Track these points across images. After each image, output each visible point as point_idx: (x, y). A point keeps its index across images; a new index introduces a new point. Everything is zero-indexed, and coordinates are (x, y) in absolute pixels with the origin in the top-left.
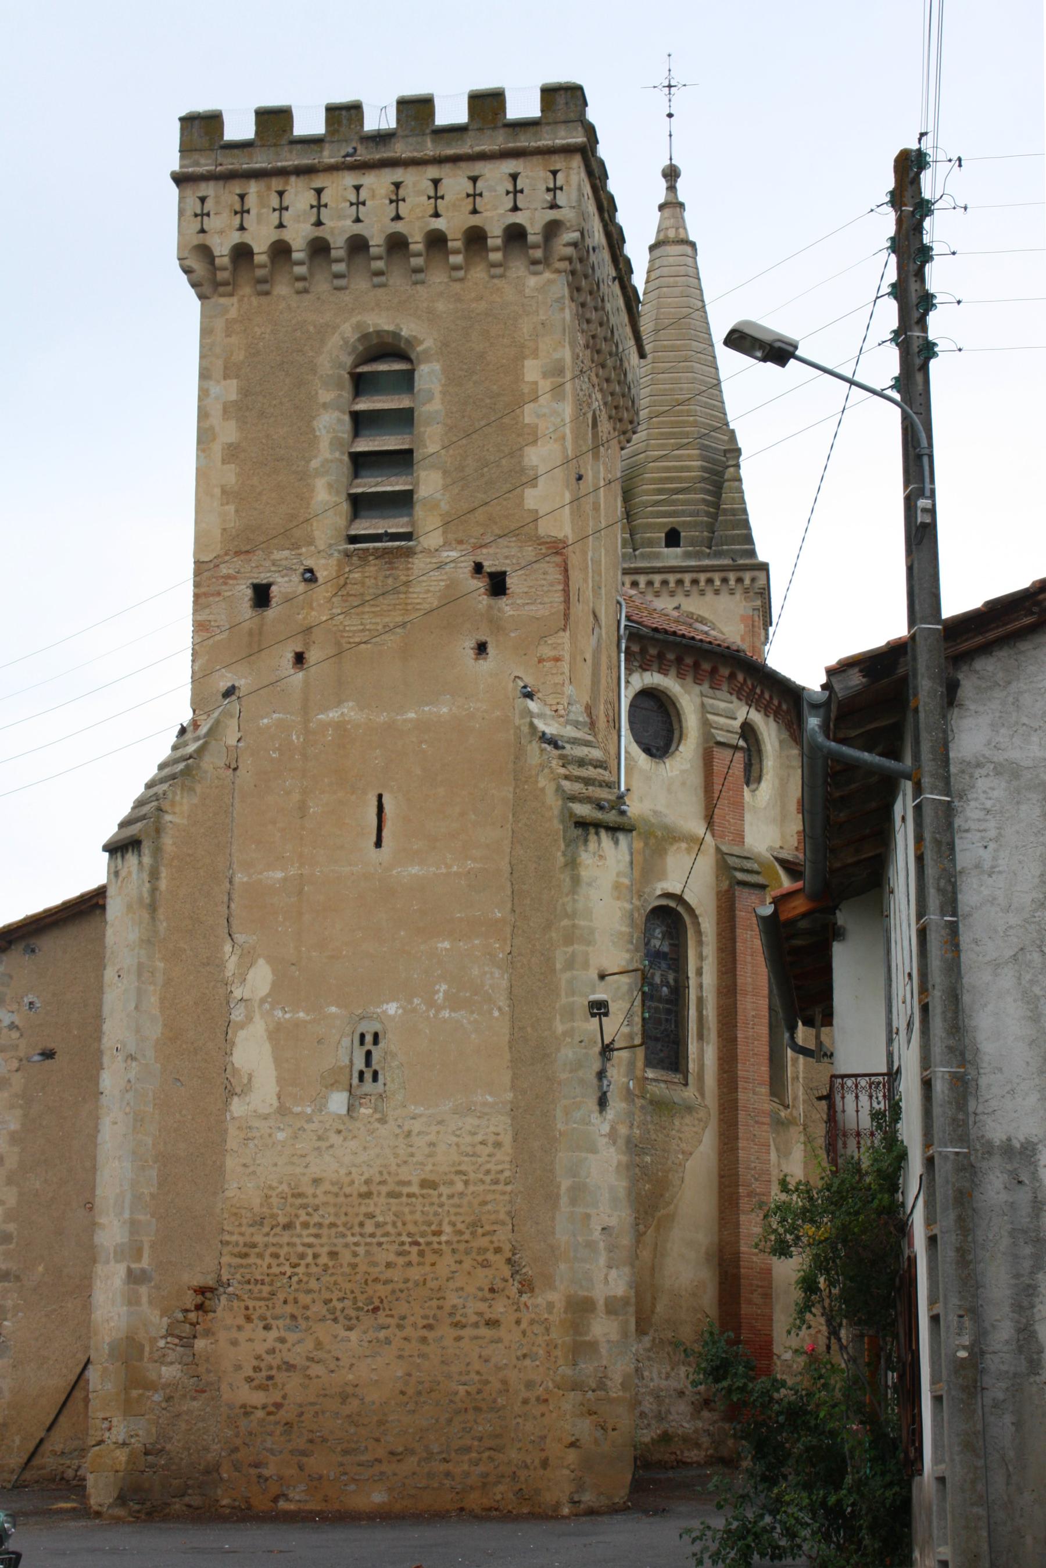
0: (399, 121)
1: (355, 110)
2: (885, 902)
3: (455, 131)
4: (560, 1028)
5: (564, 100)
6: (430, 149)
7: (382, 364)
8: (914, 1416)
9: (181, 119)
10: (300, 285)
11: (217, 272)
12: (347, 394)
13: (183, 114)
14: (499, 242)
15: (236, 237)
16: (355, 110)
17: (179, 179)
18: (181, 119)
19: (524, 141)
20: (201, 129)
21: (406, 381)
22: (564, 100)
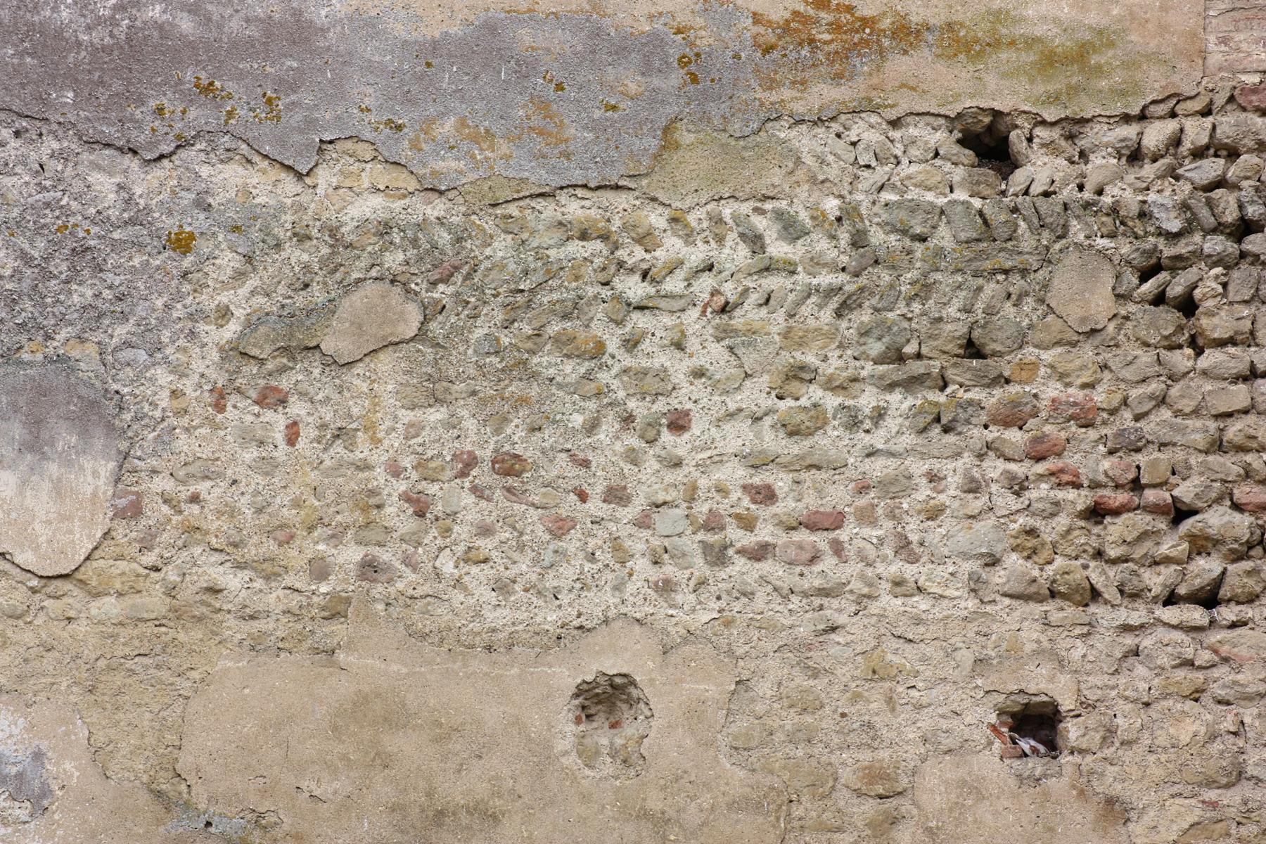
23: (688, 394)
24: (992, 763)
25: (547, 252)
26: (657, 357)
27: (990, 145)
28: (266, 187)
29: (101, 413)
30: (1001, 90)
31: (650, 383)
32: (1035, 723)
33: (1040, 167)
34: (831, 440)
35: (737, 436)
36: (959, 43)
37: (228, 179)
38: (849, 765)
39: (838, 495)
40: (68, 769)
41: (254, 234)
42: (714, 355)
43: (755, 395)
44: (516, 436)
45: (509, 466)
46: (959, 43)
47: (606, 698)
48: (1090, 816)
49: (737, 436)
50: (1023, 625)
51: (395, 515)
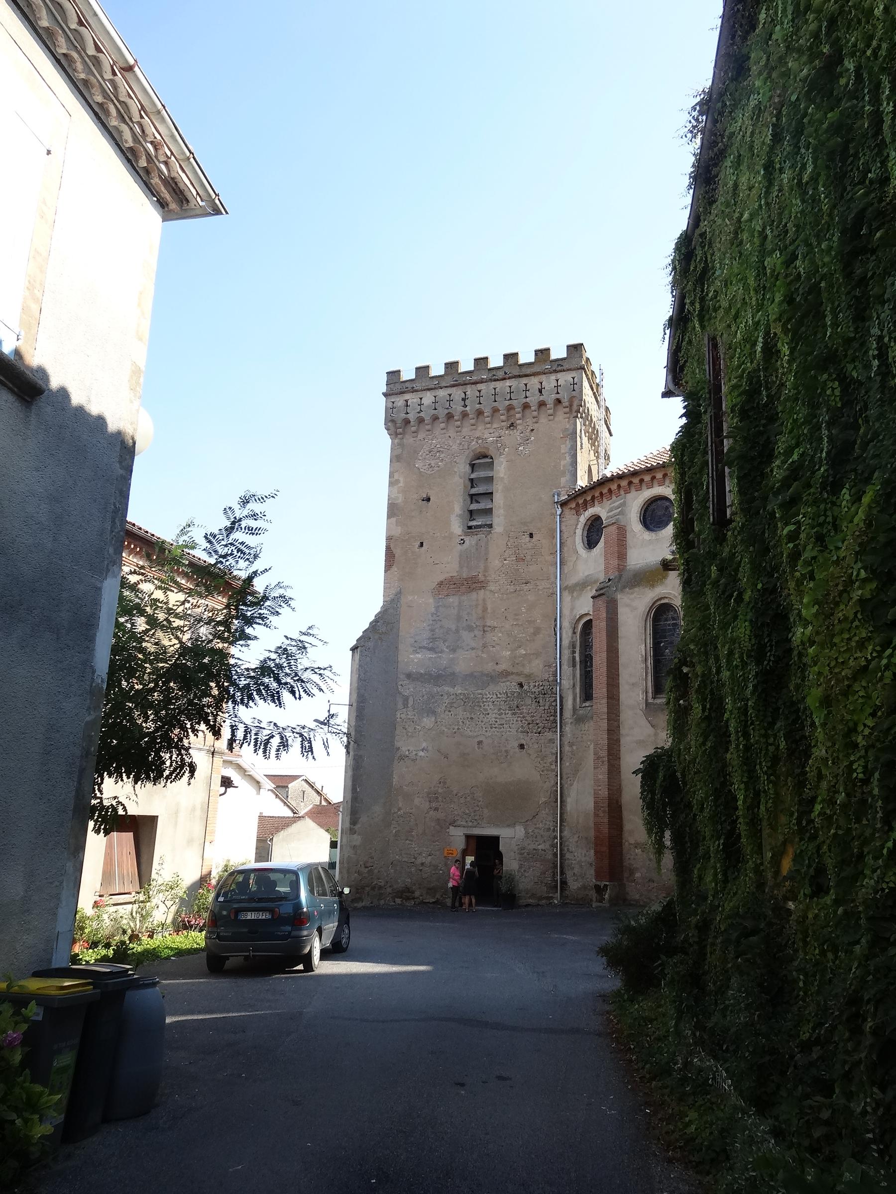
0: (504, 363)
1: (456, 364)
2: (355, 696)
3: (530, 364)
4: (887, 891)
5: (576, 349)
6: (516, 372)
7: (481, 460)
8: (76, 878)
9: (568, 347)
10: (535, 420)
11: (398, 425)
12: (468, 469)
13: (448, 361)
14: (552, 406)
15: (403, 416)
16: (485, 359)
17: (385, 395)
18: (568, 347)
19: (528, 371)
20: (393, 375)
21: (491, 465)
22: (576, 349)
23: (489, 711)
24: (517, 750)
25: (191, 552)
26: (486, 707)
27: (521, 685)
28: (451, 690)
29: (434, 713)
30: (522, 680)
31: (486, 710)
32: (522, 746)
33: (525, 687)
34: (503, 716)
35: (494, 715)
36: (518, 674)
37: (446, 688)
38: (504, 749)
39: (503, 722)
40: (430, 748)
41: (449, 694)
42: (492, 707)
43: (496, 711)
44: (473, 716)
45: (472, 718)
46: (518, 674)
47: (480, 743)
48: (521, 886)
49: (494, 715)
50: (521, 735)
51: (461, 723)
